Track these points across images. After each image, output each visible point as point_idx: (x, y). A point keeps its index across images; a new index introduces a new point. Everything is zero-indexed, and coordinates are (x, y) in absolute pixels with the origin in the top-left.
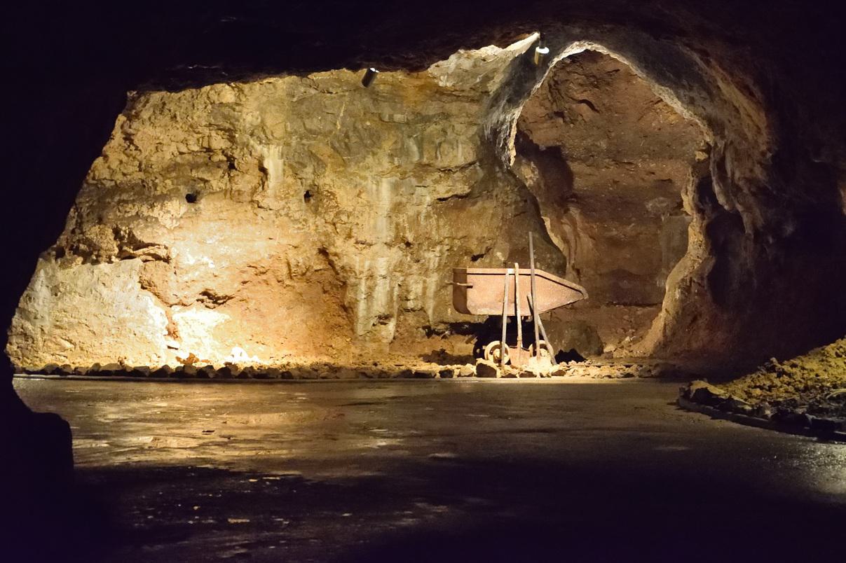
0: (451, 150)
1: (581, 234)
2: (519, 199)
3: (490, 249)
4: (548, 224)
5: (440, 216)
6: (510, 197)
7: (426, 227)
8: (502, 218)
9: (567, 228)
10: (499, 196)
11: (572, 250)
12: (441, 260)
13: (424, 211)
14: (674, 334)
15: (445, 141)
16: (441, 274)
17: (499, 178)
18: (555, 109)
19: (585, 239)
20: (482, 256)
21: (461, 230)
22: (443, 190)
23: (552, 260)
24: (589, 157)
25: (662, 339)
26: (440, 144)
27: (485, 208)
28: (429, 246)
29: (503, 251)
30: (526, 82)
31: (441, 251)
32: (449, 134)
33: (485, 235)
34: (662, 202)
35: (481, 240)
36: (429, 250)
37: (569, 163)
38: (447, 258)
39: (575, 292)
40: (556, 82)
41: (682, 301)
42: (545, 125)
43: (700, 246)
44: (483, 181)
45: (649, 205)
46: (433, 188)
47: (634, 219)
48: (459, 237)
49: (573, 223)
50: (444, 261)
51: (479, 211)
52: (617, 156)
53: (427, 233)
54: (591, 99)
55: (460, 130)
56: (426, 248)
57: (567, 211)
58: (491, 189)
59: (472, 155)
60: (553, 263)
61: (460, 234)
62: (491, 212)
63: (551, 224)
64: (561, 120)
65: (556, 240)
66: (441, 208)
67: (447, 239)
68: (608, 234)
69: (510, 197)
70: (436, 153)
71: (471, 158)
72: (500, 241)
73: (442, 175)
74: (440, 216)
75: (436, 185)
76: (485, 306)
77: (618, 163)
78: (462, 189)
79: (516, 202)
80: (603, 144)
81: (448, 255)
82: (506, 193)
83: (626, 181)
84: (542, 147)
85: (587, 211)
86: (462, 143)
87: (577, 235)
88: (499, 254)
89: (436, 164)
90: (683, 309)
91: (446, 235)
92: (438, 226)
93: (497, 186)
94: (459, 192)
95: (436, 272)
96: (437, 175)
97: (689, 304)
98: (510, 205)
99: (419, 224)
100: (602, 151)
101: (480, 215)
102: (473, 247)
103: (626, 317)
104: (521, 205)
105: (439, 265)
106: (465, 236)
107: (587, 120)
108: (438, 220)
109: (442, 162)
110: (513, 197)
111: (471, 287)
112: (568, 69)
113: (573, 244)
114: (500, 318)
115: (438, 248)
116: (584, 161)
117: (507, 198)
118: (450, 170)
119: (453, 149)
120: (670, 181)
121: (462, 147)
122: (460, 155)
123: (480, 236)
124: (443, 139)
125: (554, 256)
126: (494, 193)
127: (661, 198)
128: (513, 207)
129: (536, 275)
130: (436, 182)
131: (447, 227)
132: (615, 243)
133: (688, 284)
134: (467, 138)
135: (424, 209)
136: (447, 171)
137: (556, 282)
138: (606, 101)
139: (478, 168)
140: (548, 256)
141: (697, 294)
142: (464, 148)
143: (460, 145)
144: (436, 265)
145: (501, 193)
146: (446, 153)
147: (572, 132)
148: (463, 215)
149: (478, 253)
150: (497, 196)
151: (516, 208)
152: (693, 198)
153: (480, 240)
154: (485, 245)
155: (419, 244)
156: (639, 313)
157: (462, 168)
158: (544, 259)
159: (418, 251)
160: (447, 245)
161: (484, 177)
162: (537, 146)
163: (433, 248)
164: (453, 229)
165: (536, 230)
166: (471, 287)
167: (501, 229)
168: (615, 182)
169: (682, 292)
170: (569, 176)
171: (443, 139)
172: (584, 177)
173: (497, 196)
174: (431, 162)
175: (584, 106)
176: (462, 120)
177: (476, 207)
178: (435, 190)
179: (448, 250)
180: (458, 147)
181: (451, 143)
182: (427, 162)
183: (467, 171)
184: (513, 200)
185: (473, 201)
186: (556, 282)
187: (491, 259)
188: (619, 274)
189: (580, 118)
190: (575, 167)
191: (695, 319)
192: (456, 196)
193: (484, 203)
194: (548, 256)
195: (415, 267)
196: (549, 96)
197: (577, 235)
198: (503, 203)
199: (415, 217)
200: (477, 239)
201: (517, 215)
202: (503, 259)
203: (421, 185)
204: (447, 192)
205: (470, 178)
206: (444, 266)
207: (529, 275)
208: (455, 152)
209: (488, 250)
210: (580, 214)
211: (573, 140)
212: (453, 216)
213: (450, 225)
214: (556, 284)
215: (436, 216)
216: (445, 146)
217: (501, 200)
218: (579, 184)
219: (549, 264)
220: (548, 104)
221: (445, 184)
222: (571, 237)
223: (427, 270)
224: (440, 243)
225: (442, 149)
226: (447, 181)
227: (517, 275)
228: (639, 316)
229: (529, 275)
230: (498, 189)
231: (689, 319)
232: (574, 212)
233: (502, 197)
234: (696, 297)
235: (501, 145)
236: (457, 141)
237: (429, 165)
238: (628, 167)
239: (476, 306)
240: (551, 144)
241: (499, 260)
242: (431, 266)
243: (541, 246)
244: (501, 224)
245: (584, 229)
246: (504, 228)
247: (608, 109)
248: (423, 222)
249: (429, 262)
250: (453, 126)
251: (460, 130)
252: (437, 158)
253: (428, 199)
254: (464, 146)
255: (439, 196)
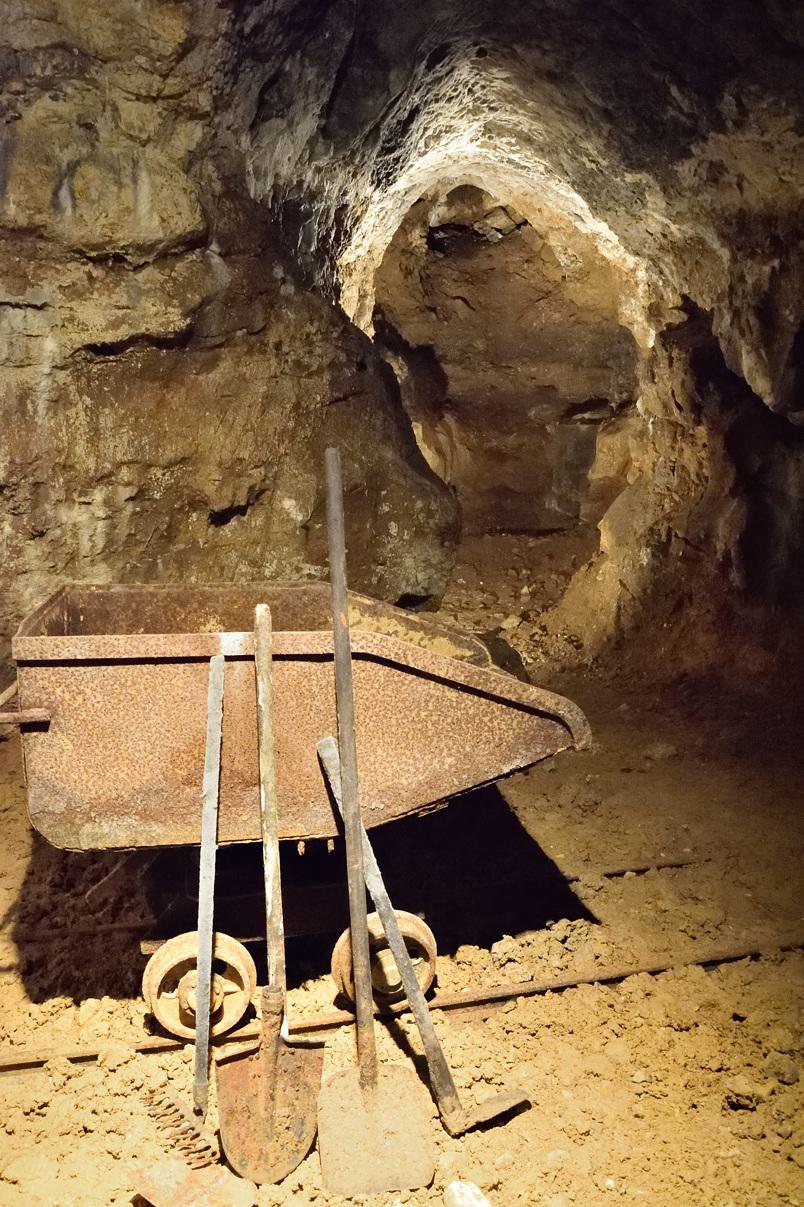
0: (115, 189)
1: (457, 445)
2: (343, 357)
3: (262, 492)
4: (418, 431)
5: (100, 400)
6: (318, 351)
7: (54, 432)
8: (297, 407)
9: (442, 438)
10: (285, 349)
11: (448, 464)
12: (114, 527)
13: (45, 383)
14: (637, 628)
15: (92, 158)
16: (120, 565)
17: (288, 299)
18: (428, 303)
19: (461, 449)
20: (241, 511)
21: (171, 442)
22: (97, 319)
23: (430, 514)
24: (462, 360)
25: (611, 630)
26: (73, 167)
27: (243, 378)
28: (69, 491)
29: (299, 496)
30: (366, 95)
31: (107, 502)
32: (104, 134)
33: (245, 454)
34: (547, 410)
35: (232, 469)
36: (69, 500)
37: (442, 365)
38: (130, 521)
39: (536, 720)
40: (428, 276)
41: (654, 569)
42: (416, 319)
43: (673, 471)
44: (230, 299)
45: (194, 515)
46: (67, 314)
47: (515, 428)
48: (163, 461)
49: (449, 434)
50: (123, 531)
51: (227, 385)
52: (497, 359)
53: (59, 451)
54: (466, 295)
55: (137, 123)
56: (62, 495)
57: (441, 417)
58: (260, 325)
59: (185, 208)
60: (431, 522)
61: (169, 452)
62: (263, 389)
63: (423, 433)
64: (434, 315)
65: (429, 455)
66: (103, 376)
67: (124, 470)
68: (487, 445)
69: (318, 351)
70: (56, 193)
71: (186, 221)
72: (290, 467)
73: (97, 272)
74: (100, 400)
75: (73, 304)
76: (115, 808)
77: (495, 365)
78: (162, 317)
79: (332, 365)
80: (480, 345)
81: (135, 513)
82: (308, 341)
83: (506, 386)
84: (413, 344)
85: (464, 420)
86: (151, 171)
87: (453, 447)
88: (289, 504)
89: (60, 228)
90: (656, 583)
91: (119, 457)
92: (96, 430)
93: (279, 318)
94: (154, 327)
95: (104, 560)
96: (75, 272)
97: (665, 575)
98: (320, 371)
99: (31, 426)
100: (479, 353)
101: (226, 399)
102: (210, 489)
103: (515, 551)
104: (348, 373)
105: (110, 541)
106: (184, 459)
107: (462, 318)
108: (93, 413)
109: (78, 224)
110: (322, 353)
111: (42, 726)
112: (440, 263)
113: (449, 458)
114: (191, 852)
115: (98, 495)
116: (460, 362)
117: (310, 352)
118: (119, 259)
119: (120, 186)
120: (553, 387)
121: (153, 185)
122: (144, 206)
123: (226, 455)
124: (85, 150)
125: (434, 506)
126: (272, 338)
127: (545, 406)
128: (327, 377)
129: (357, 656)
130: (73, 292)
131: (126, 434)
132: (498, 456)
133: (664, 538)
134: (171, 159)
135: (42, 380)
136: (111, 260)
137: (452, 684)
138: (482, 299)
139: (216, 260)
140: (419, 504)
141: (681, 559)
142: (156, 189)
143: (143, 175)
144: (100, 543)
145: (293, 338)
146: (94, 195)
147: (446, 332)
148: (176, 398)
149: (226, 505)
150: (278, 346)
151: (333, 383)
152: (683, 383)
153: (231, 468)
154: (247, 483)
155: (37, 484)
156: (531, 544)
157: (164, 254)
158: (410, 514)
159: (35, 504)
160: (128, 484)
161: (231, 283)
162: (407, 343)
163: (83, 493)
164: (145, 440)
165: (389, 437)
166: (42, 726)
167: (292, 438)
168: (493, 387)
169: (653, 555)
170: (442, 380)
171: (85, 150)
172: (459, 380)
173: (278, 346)
174: (39, 219)
175: (460, 301)
176: (139, 81)
177: (216, 376)
178: (71, 319)
179: (131, 499)
180: (135, 180)
181: (113, 169)
182: (23, 221)
183: (180, 266)
184: (326, 361)
185: (203, 356)
186: (452, 684)
187: (268, 519)
188: (502, 492)
189: (454, 316)
190: (448, 369)
191: (679, 606)
192: (147, 339)
193: (237, 364)
194: (419, 504)
195: (33, 551)
196: (420, 287)
197: (453, 447)
198: (298, 363)
199: (13, 402)
200: (220, 464)
201: (337, 400)
202: (300, 518)
203: (19, 299)
204: (115, 325)
205: (188, 285)
206: (126, 543)
207: (328, 657)
208: (127, 195)
209: (256, 495)
210: (457, 421)
211: (446, 340)
212: (147, 401)
213: (135, 427)
214: (452, 694)
215: (88, 401)
216: (90, 172)
217: (291, 358)
218: (454, 388)
219: (420, 526)
220: (419, 296)
221: (105, 300)
222: (447, 448)
223: (73, 557)
224: (104, 479)
225: (78, 183)
226: (111, 292)
227: (263, 660)
228: (531, 548)
229: (328, 657)
230: (281, 327)
231: (670, 604)
232: (449, 418)
233: (295, 351)
234: (679, 564)
235: (312, 249)
236: (135, 163)
237: (33, 231)
238: (508, 371)
239: (70, 810)
240: (422, 342)
241: (290, 520)
242: (85, 546)
243: (402, 481)
244: (291, 424)
245: (462, 441)
246: (302, 434)
247: (485, 308)
248: (43, 418)
249: (75, 535)
250: (116, 109)
251: (137, 123)
252: (56, 205)
253: (50, 346)
254: (160, 180)
255: (87, 338)
